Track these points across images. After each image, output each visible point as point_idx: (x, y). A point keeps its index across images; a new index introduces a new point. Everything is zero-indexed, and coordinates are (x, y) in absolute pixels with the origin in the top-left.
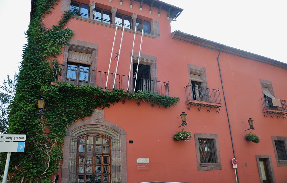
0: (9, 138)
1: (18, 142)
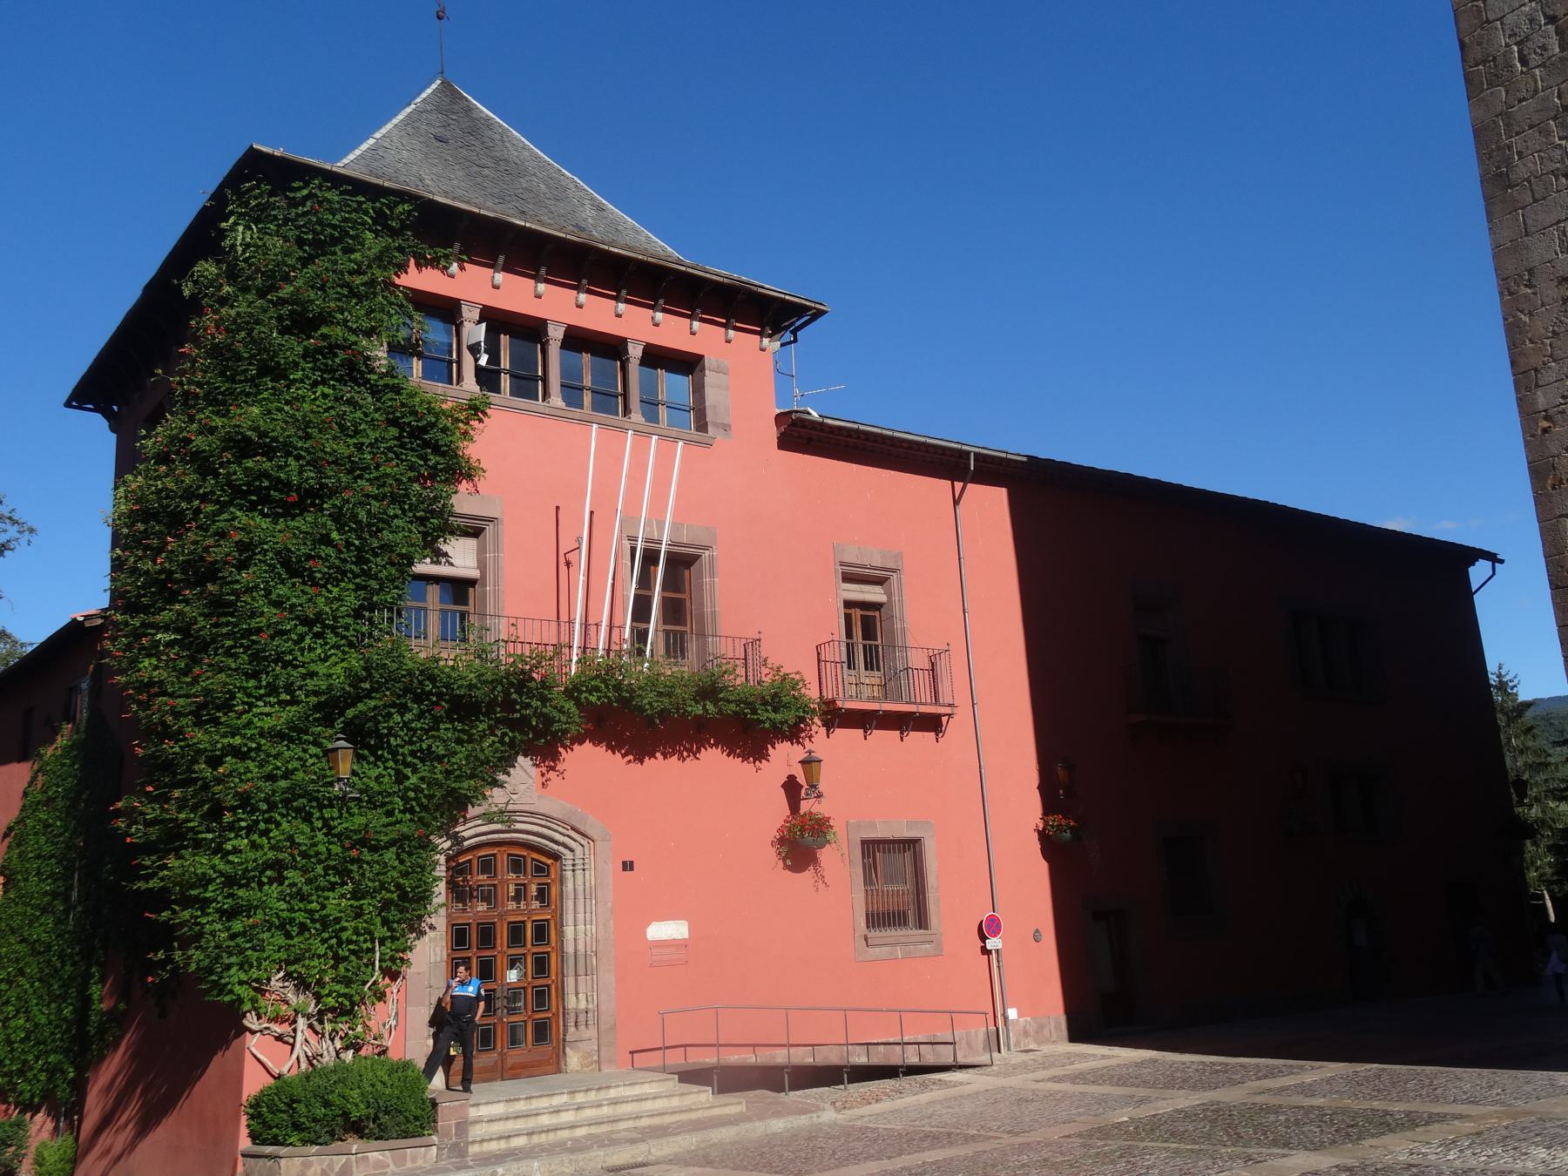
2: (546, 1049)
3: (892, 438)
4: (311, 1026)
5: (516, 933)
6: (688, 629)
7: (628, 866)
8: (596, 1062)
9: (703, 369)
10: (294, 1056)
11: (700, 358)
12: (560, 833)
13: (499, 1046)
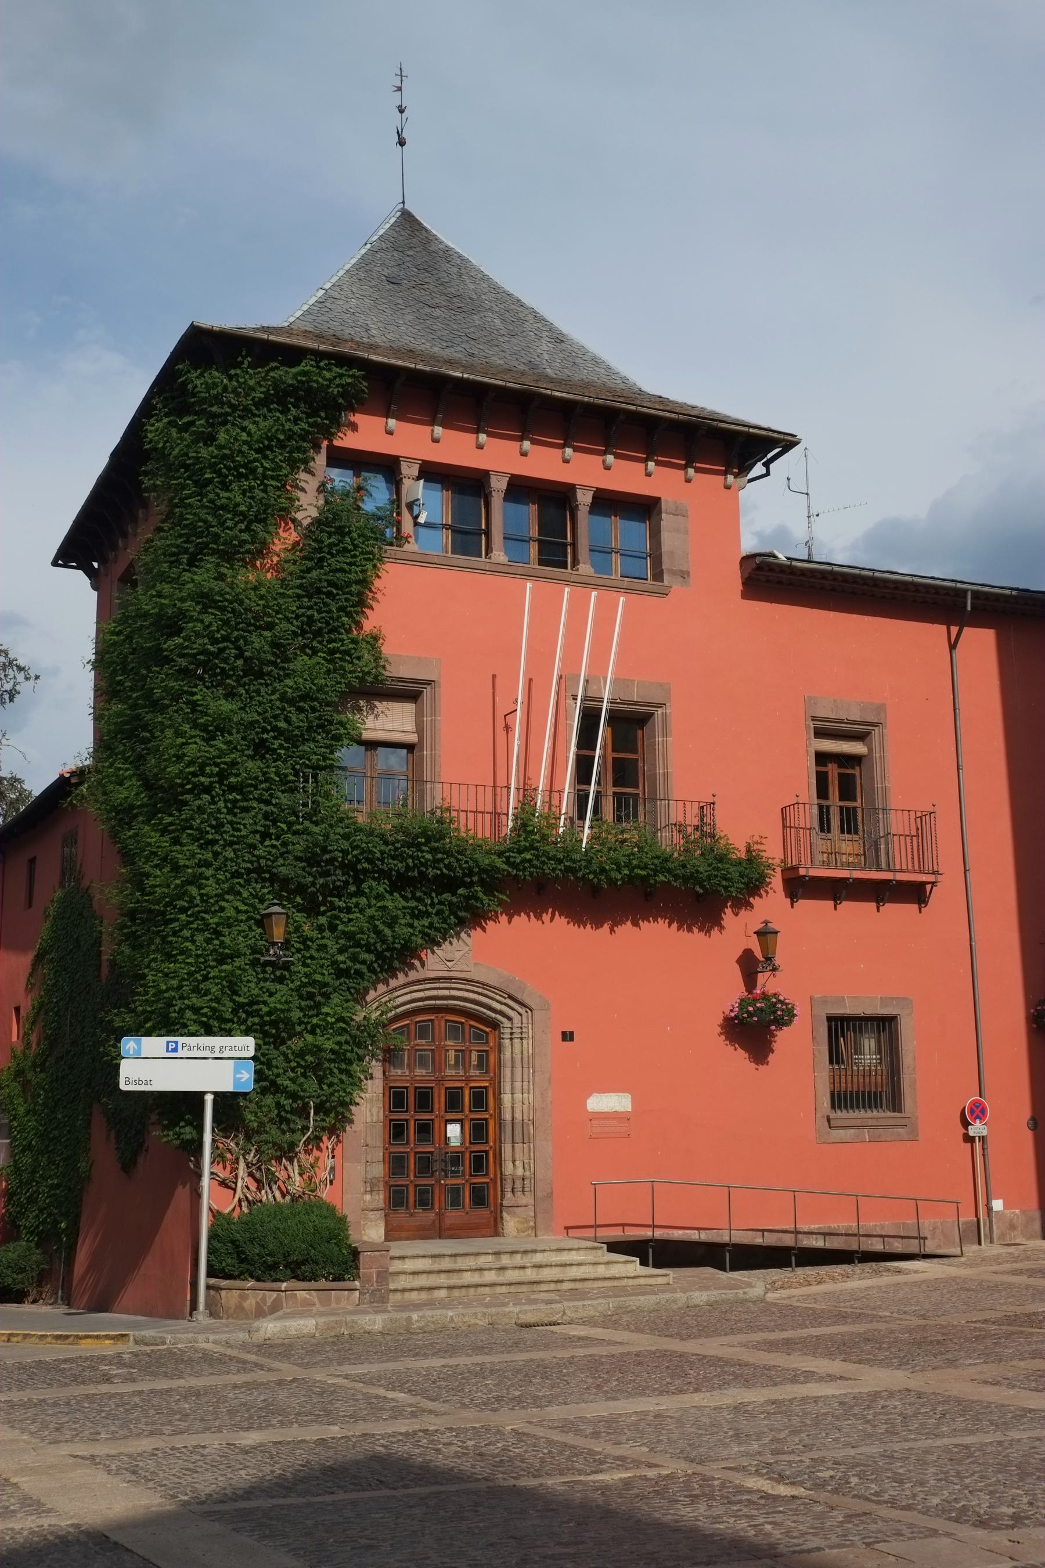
0: (205, 1048)
1: (232, 1061)
2: (484, 1213)
3: (873, 578)
4: (251, 1174)
5: (454, 1100)
6: (640, 791)
7: (568, 1036)
8: (532, 1227)
9: (660, 513)
10: (236, 1200)
11: (657, 500)
12: (498, 1001)
13: (437, 1206)
